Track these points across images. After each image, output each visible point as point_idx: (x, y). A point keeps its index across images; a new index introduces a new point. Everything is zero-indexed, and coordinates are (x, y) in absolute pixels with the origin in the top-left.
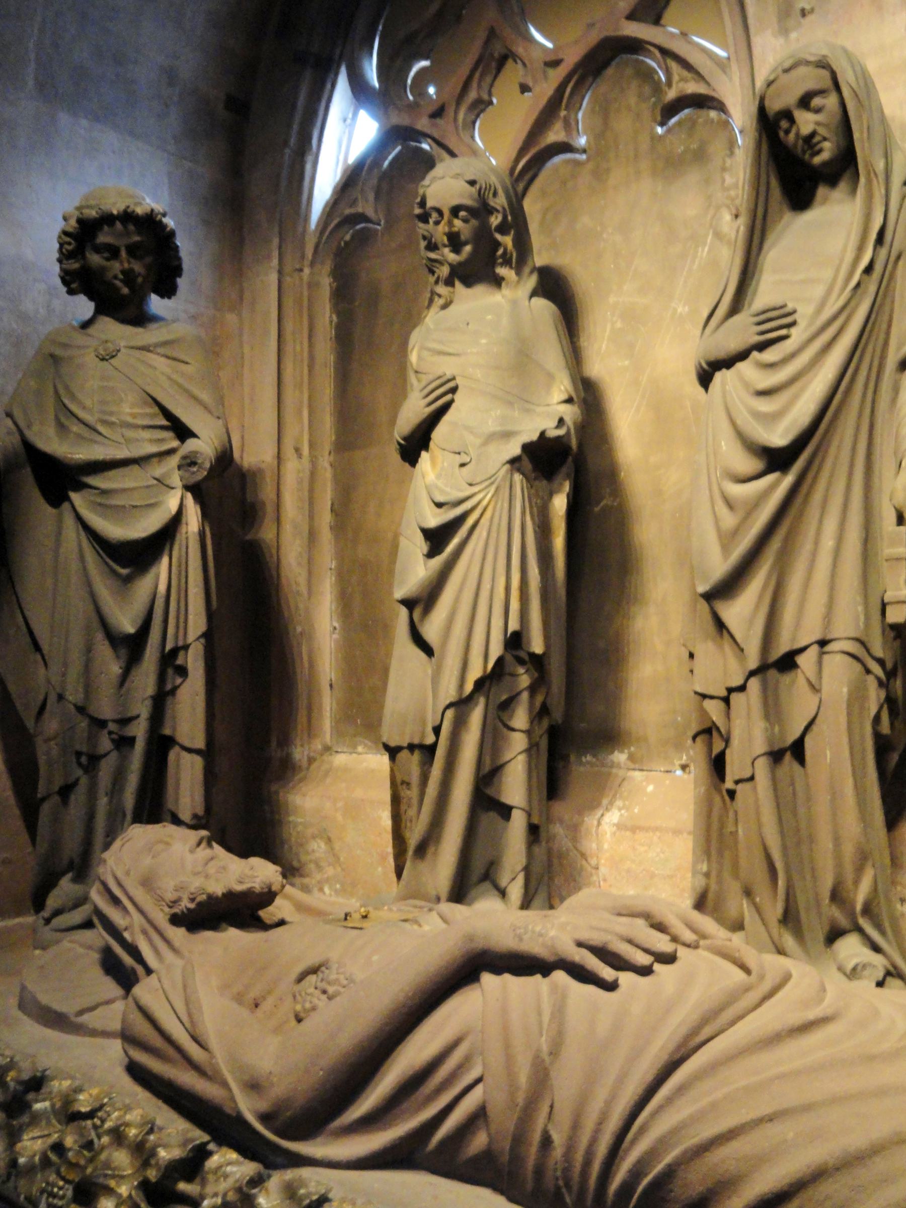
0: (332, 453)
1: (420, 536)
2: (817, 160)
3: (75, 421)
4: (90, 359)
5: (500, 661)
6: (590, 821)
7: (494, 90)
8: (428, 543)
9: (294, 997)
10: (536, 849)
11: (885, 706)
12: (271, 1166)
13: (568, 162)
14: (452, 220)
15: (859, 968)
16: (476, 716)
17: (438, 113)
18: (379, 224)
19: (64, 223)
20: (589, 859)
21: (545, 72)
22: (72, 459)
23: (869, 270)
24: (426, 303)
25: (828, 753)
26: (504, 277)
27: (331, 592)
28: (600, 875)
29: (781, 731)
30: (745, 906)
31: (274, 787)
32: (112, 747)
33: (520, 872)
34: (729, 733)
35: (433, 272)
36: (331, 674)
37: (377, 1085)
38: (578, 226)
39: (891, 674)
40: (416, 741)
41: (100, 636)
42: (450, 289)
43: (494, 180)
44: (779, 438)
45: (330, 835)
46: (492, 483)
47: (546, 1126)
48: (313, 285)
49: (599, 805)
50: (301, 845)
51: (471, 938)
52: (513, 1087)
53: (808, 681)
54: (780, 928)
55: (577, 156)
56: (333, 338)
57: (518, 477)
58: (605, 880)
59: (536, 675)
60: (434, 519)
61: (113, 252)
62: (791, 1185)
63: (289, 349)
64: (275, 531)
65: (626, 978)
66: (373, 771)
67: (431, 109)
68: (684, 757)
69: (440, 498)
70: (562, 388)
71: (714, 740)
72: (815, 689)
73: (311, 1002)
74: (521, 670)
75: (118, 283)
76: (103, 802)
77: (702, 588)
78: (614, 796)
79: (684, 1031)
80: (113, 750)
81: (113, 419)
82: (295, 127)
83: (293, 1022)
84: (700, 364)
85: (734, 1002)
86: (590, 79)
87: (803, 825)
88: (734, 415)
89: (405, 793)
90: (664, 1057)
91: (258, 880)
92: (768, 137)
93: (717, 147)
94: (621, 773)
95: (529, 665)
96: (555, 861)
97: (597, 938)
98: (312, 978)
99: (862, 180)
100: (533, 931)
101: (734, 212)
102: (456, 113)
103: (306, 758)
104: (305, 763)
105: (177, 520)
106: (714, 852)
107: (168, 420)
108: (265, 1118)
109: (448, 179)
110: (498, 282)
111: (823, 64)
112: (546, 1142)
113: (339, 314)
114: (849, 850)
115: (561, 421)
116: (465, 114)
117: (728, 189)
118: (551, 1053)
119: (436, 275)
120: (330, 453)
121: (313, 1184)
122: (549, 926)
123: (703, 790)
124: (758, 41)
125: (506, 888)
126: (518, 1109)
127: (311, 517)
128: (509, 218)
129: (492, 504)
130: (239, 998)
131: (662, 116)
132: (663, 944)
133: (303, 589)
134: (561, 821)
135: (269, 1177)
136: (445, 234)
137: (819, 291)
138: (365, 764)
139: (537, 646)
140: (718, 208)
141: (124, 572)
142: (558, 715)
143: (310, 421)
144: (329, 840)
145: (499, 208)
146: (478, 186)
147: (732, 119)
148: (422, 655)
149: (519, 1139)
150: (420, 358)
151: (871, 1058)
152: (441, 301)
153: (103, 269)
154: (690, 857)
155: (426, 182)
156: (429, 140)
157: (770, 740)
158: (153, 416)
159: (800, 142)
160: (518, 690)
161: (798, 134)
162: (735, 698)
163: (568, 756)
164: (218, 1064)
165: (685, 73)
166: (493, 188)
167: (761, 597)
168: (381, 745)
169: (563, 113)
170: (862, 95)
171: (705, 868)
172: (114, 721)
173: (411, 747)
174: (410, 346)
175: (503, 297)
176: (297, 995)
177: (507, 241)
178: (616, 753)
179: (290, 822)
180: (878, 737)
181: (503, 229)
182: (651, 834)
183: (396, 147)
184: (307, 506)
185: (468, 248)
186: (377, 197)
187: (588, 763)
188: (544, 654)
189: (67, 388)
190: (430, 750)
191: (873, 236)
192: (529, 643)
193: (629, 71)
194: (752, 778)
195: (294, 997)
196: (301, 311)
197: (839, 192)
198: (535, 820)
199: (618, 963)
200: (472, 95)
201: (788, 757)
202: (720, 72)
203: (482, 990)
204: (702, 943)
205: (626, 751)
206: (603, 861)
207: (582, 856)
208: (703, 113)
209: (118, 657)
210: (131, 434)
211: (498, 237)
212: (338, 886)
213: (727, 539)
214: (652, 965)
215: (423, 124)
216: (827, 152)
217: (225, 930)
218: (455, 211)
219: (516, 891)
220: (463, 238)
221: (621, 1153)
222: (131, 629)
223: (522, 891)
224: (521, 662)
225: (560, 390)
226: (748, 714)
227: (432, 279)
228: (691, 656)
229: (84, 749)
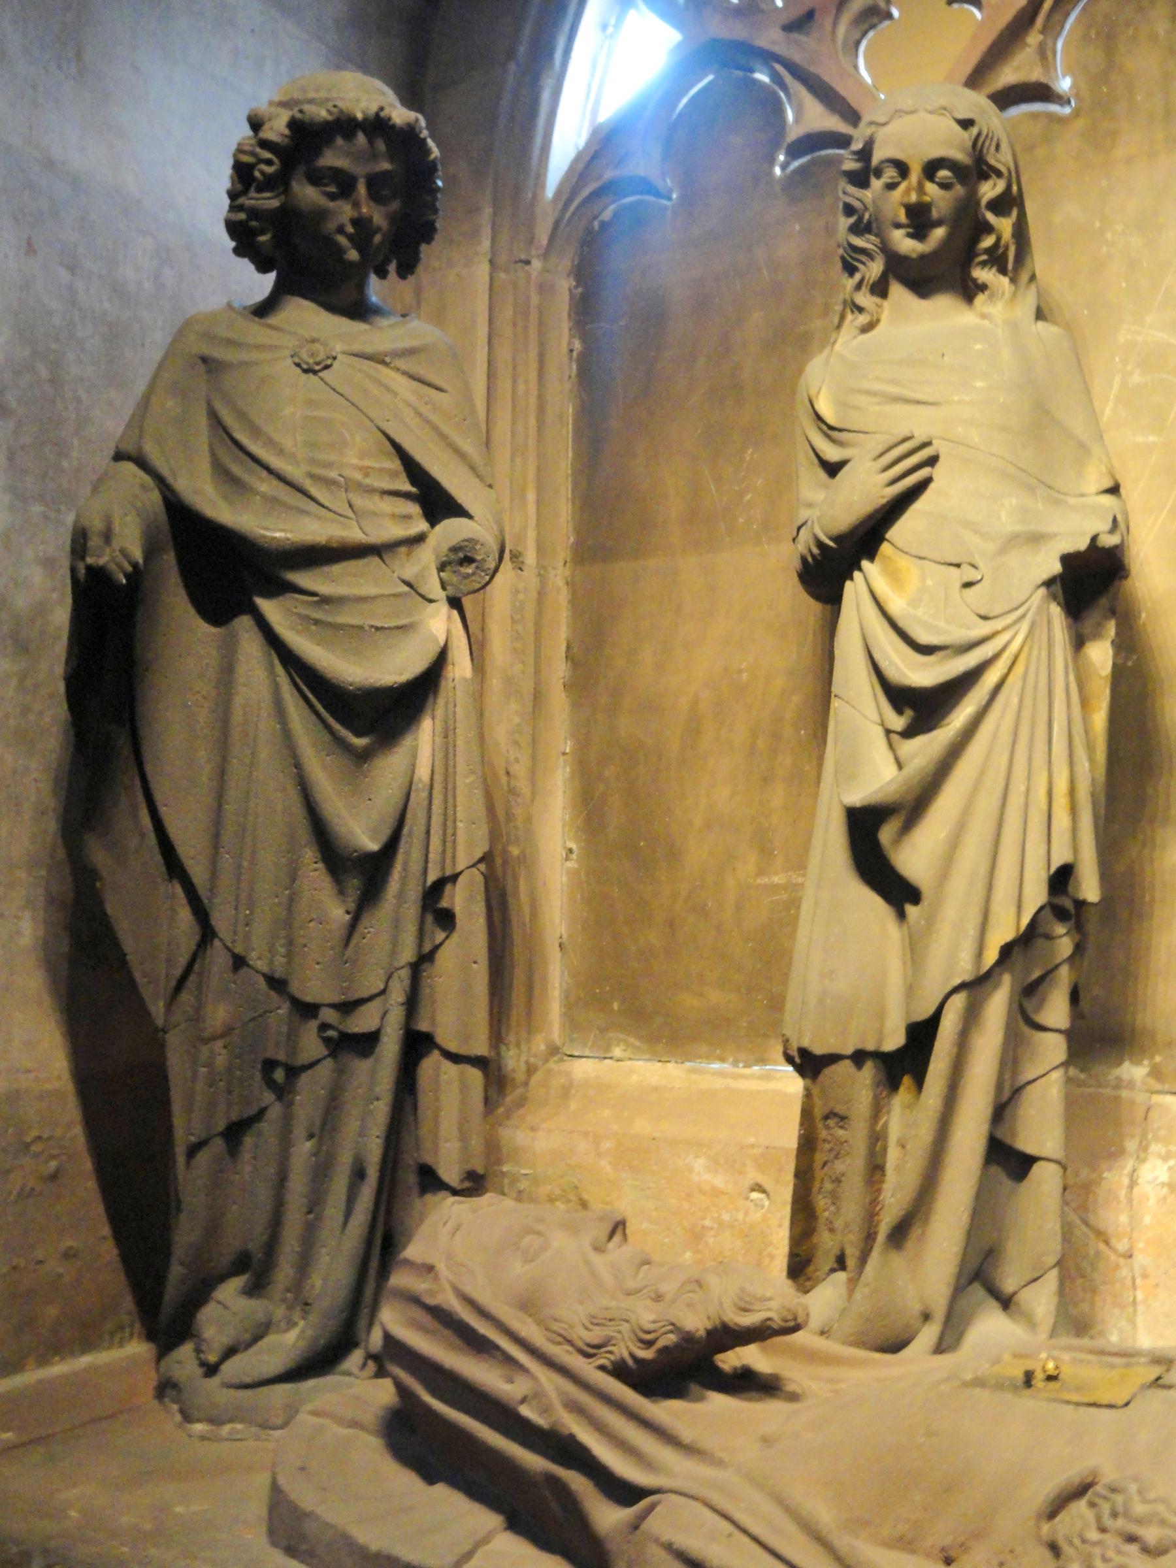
0: (568, 564)
3: (264, 474)
4: (285, 368)
13: (1035, 116)
16: (998, 1004)
18: (670, 199)
19: (249, 132)
20: (1113, 1241)
22: (265, 537)
26: (988, 284)
28: (1136, 1268)
32: (326, 1053)
33: (1054, 1266)
40: (870, 1047)
41: (310, 855)
45: (585, 1196)
46: (1023, 617)
48: (546, 289)
55: (1053, 108)
58: (1145, 1276)
61: (344, 185)
66: (656, 1089)
74: (1060, 929)
75: (342, 240)
76: (304, 1148)
78: (1144, 1136)
80: (324, 1058)
81: (333, 474)
91: (774, 1304)
94: (1140, 1097)
102: (835, 24)
103: (523, 1067)
104: (520, 1076)
105: (441, 659)
107: (413, 484)
110: (969, 291)
116: (847, 31)
119: (858, 276)
120: (565, 563)
125: (1015, 1293)
129: (1026, 649)
141: (360, 742)
152: (863, 319)
153: (321, 215)
158: (393, 475)
166: (995, 139)
172: (333, 1006)
173: (859, 1057)
177: (1005, 225)
178: (1126, 1065)
179: (503, 1174)
183: (706, 76)
185: (939, 233)
189: (242, 416)
205: (1146, 1062)
206: (1141, 1245)
209: (341, 892)
210: (360, 501)
211: (990, 217)
217: (700, 1399)
218: (931, 169)
222: (374, 846)
223: (1055, 1299)
227: (850, 283)
229: (281, 1056)
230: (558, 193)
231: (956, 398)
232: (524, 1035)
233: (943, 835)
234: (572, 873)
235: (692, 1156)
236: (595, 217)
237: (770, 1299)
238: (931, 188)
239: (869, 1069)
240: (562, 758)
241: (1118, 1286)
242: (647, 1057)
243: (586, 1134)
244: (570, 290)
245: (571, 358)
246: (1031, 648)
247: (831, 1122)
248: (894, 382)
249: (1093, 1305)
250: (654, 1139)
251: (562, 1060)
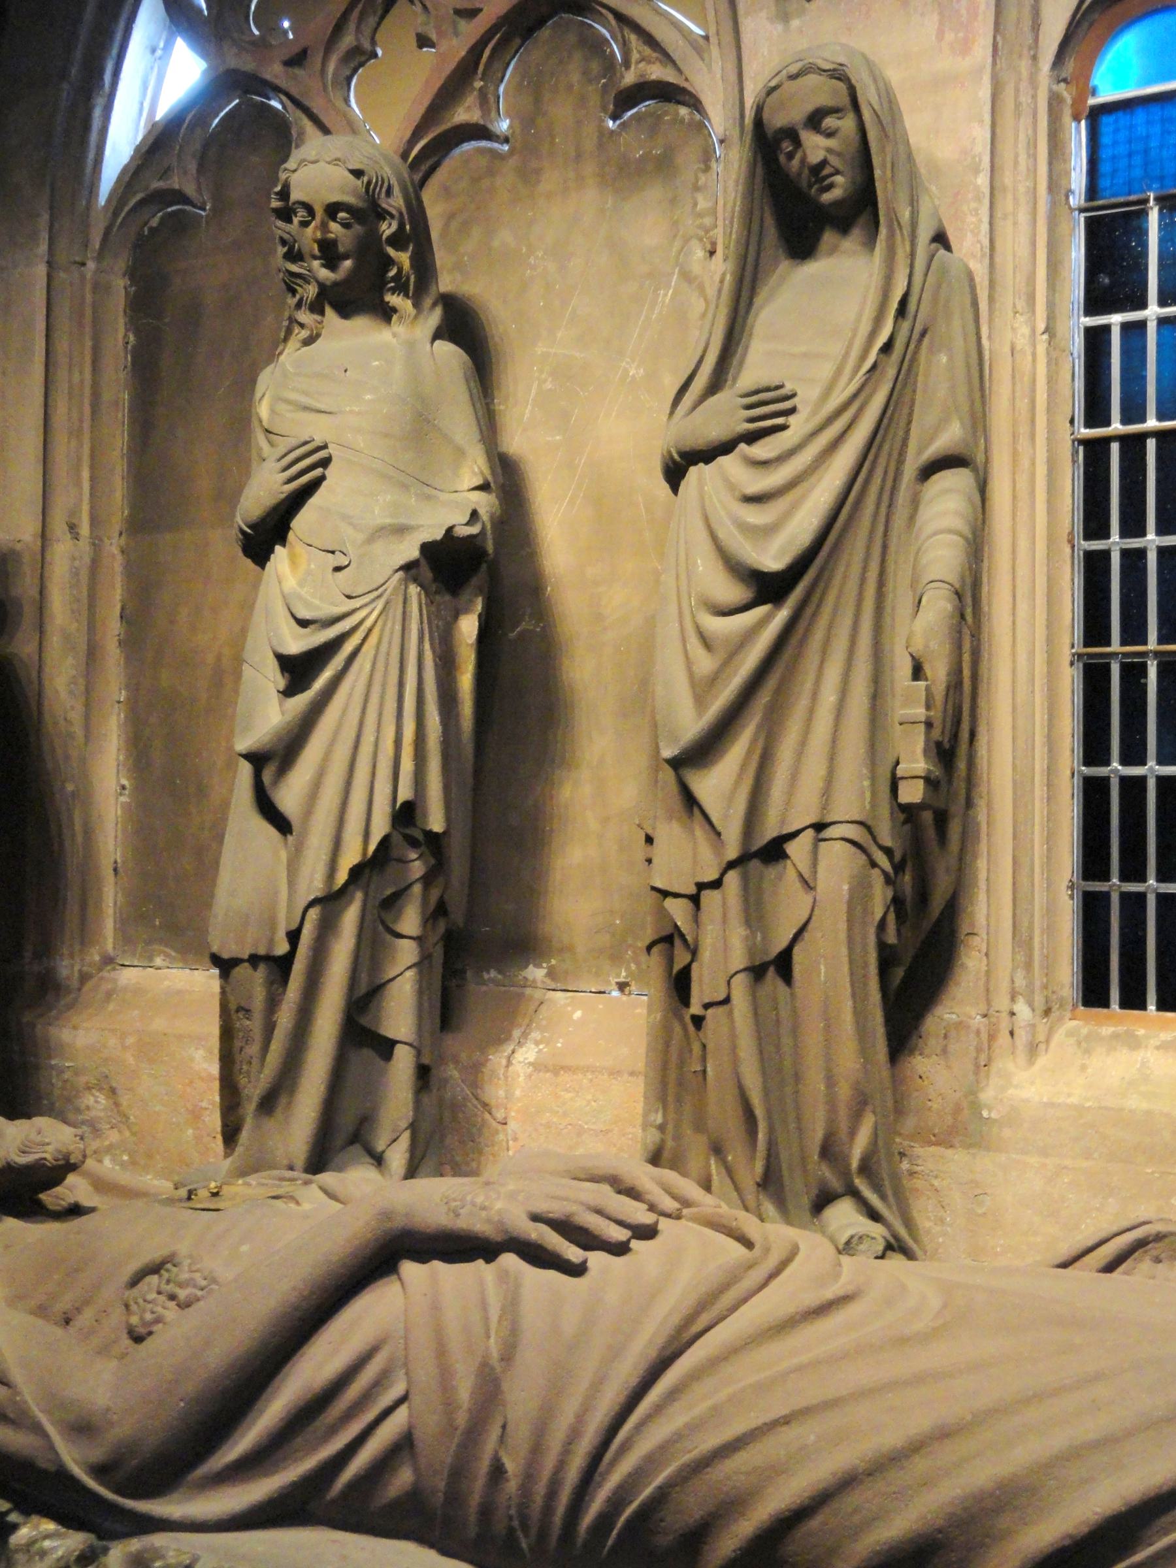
0: (124, 535)
1: (272, 666)
2: (827, 197)
5: (385, 842)
6: (497, 1059)
7: (378, 37)
8: (286, 675)
9: (127, 1306)
10: (426, 1099)
11: (892, 909)
12: (107, 1535)
14: (327, 223)
15: (855, 1241)
16: (350, 917)
17: (298, 60)
18: (204, 210)
21: (455, 25)
23: (887, 348)
24: (282, 335)
25: (822, 967)
27: (119, 735)
28: (510, 1132)
29: (764, 938)
30: (713, 1167)
31: (27, 1018)
33: (406, 1129)
34: (696, 941)
35: (293, 292)
36: (116, 854)
37: (261, 1412)
38: (496, 243)
39: (899, 868)
40: (262, 951)
42: (318, 318)
43: (387, 172)
44: (773, 559)
46: (379, 597)
47: (496, 1452)
49: (508, 1038)
50: (69, 1100)
51: (386, 1215)
52: (449, 1405)
53: (801, 876)
54: (758, 1192)
55: (496, 145)
56: (129, 368)
57: (414, 590)
58: (515, 1139)
59: (433, 861)
60: (296, 643)
62: (813, 1498)
63: (61, 375)
64: (36, 644)
65: (597, 1260)
66: (179, 992)
67: (286, 54)
68: (624, 974)
69: (304, 614)
70: (476, 470)
71: (676, 952)
72: (808, 885)
73: (153, 1312)
74: (413, 855)
77: (668, 753)
79: (676, 1320)
82: (78, 54)
83: (127, 1342)
84: (669, 452)
85: (736, 1282)
86: (518, 41)
87: (788, 1063)
88: (715, 526)
89: (241, 1022)
90: (653, 1353)
91: (50, 1148)
92: (763, 158)
93: (688, 158)
94: (538, 994)
95: (423, 848)
96: (447, 1114)
97: (556, 1209)
98: (153, 1279)
99: (883, 231)
100: (473, 1204)
101: (709, 247)
103: (76, 975)
104: (75, 983)
106: (670, 1099)
108: (100, 1471)
109: (322, 164)
110: (386, 314)
111: (838, 74)
112: (497, 1471)
113: (138, 332)
114: (844, 1091)
115: (474, 514)
116: (337, 69)
117: (700, 215)
118: (502, 1359)
119: (298, 297)
120: (121, 534)
121: (171, 1553)
122: (494, 1195)
123: (659, 1016)
124: (748, 25)
125: (383, 1152)
126: (459, 1432)
127: (92, 627)
128: (408, 227)
129: (380, 623)
130: (41, 1311)
131: (616, 105)
132: (640, 1215)
133: (78, 730)
134: (456, 1062)
135: (106, 1550)
136: (316, 241)
137: (826, 370)
138: (167, 983)
139: (436, 823)
140: (687, 241)
142: (458, 916)
143: (92, 488)
144: (113, 1091)
145: (394, 212)
146: (365, 179)
147: (709, 121)
148: (270, 831)
149: (458, 1473)
150: (273, 411)
151: (902, 1341)
152: (304, 334)
154: (639, 1107)
155: (291, 164)
156: (284, 98)
157: (751, 951)
159: (806, 171)
160: (410, 882)
161: (803, 161)
162: (708, 896)
163: (464, 972)
164: (26, 1402)
165: (647, 51)
166: (386, 185)
167: (743, 767)
168: (207, 960)
169: (478, 84)
170: (886, 119)
171: (659, 1119)
173: (254, 960)
174: (258, 395)
175: (394, 335)
176: (132, 1303)
177: (404, 258)
179: (52, 1067)
180: (882, 946)
181: (397, 241)
182: (580, 1076)
184: (85, 614)
186: (201, 168)
187: (492, 980)
188: (444, 833)
190: (282, 966)
191: (894, 305)
192: (425, 815)
193: (572, 38)
194: (727, 1001)
195: (127, 1306)
196: (81, 325)
197: (851, 243)
198: (426, 1060)
199: (588, 1240)
200: (348, 40)
201: (771, 972)
202: (697, 57)
203: (402, 1284)
204: (685, 1211)
206: (513, 1114)
207: (483, 1107)
208: (670, 107)
211: (391, 251)
212: (125, 1158)
213: (702, 690)
214: (629, 1241)
215: (274, 72)
216: (839, 188)
218: (332, 210)
219: (397, 1157)
220: (341, 249)
221: (597, 1478)
223: (407, 1155)
224: (413, 843)
225: (474, 473)
226: (725, 915)
227: (292, 301)
228: (649, 840)
230: (109, 201)
231: (348, 409)
232: (77, 947)
233: (308, 777)
234: (126, 808)
235: (193, 1049)
236: (146, 224)
237: (48, 1144)
238: (334, 226)
239: (262, 967)
240: (117, 706)
241: (496, 1148)
242: (181, 965)
243: (113, 1031)
244: (125, 288)
245: (126, 348)
246: (384, 624)
247: (241, 1015)
248: (306, 393)
249: (479, 1163)
250: (165, 1034)
251: (114, 969)
